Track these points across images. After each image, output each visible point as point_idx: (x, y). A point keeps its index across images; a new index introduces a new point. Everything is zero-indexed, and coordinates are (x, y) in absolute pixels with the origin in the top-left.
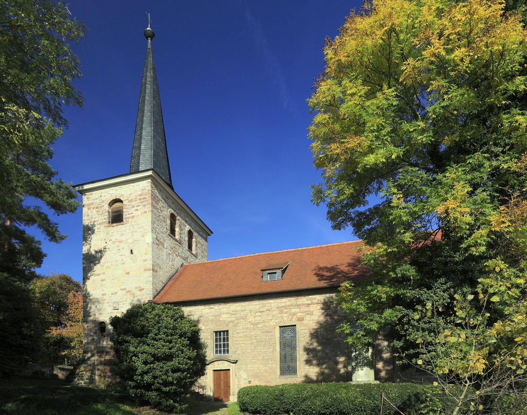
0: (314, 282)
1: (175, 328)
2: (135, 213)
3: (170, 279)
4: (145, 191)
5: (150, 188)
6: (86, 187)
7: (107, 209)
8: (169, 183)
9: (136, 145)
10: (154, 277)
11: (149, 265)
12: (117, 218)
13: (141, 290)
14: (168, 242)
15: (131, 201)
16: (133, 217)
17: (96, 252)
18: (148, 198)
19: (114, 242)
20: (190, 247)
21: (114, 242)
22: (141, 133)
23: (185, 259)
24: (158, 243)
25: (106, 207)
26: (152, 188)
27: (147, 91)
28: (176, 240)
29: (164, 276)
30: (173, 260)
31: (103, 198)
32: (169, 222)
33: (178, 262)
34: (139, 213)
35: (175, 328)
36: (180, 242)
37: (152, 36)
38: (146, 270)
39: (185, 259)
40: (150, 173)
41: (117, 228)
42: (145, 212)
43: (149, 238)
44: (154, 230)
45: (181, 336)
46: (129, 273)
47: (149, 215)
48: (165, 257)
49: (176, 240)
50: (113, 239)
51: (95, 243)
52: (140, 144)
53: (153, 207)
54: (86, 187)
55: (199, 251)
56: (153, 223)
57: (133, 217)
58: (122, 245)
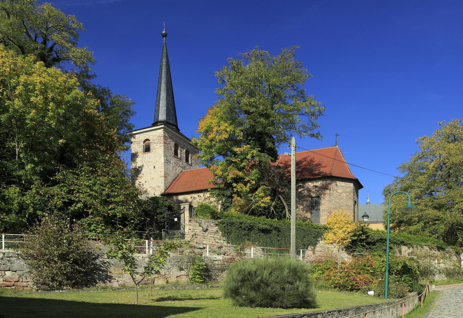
0: (209, 187)
1: (163, 204)
2: (156, 147)
3: (174, 180)
4: (161, 135)
5: (163, 133)
6: (134, 133)
7: (143, 144)
8: (175, 124)
9: (157, 104)
10: (165, 180)
11: (163, 174)
12: (147, 149)
13: (159, 187)
14: (173, 160)
15: (154, 140)
16: (155, 149)
17: (139, 167)
18: (162, 138)
19: (146, 162)
20: (187, 160)
21: (146, 162)
22: (160, 97)
23: (184, 168)
24: (167, 162)
25: (142, 143)
26: (164, 133)
27: (163, 71)
28: (178, 158)
29: (170, 179)
30: (176, 169)
31: (141, 139)
32: (173, 149)
33: (179, 170)
34: (158, 147)
35: (163, 204)
36: (180, 159)
37: (165, 35)
38: (161, 177)
39: (184, 168)
40: (163, 126)
41: (147, 155)
42: (161, 146)
43: (162, 160)
44: (165, 155)
45: (165, 207)
46: (153, 179)
47: (163, 148)
48: (171, 169)
49: (178, 158)
50: (146, 160)
51: (139, 162)
52: (159, 104)
53: (165, 143)
54: (134, 133)
55: (193, 161)
56: (165, 152)
57: (155, 149)
58: (150, 164)
